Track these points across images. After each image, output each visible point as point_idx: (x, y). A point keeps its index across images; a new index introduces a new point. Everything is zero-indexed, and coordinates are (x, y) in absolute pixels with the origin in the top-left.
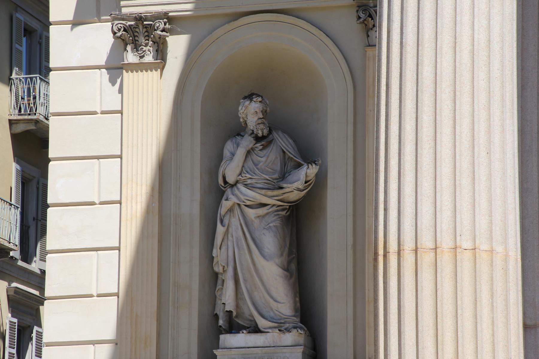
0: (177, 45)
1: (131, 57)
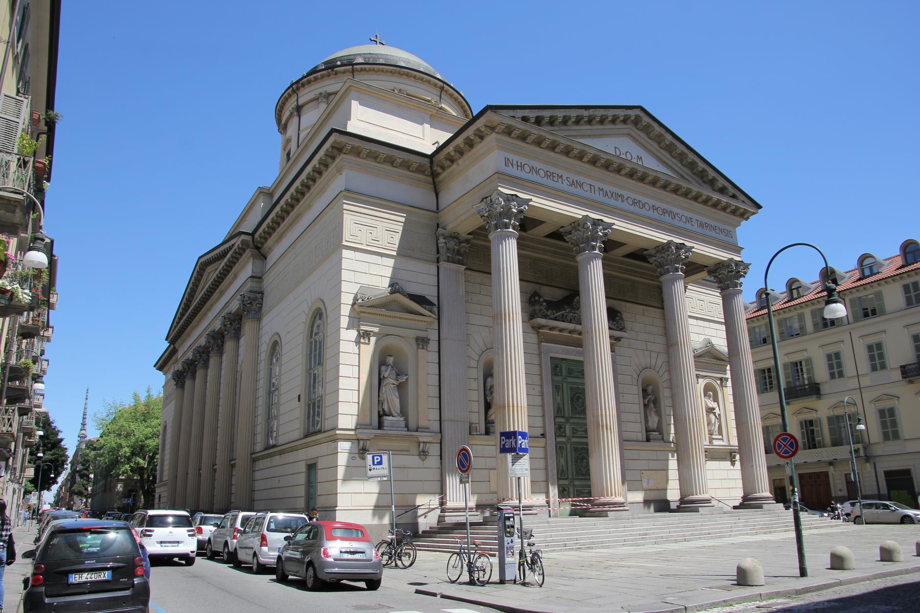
0: (373, 339)
1: (362, 340)
